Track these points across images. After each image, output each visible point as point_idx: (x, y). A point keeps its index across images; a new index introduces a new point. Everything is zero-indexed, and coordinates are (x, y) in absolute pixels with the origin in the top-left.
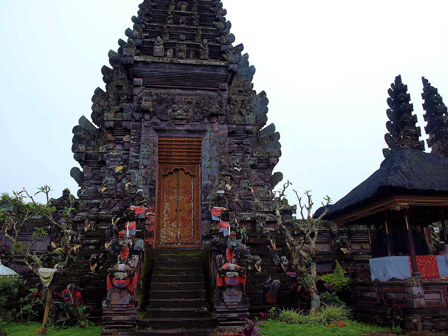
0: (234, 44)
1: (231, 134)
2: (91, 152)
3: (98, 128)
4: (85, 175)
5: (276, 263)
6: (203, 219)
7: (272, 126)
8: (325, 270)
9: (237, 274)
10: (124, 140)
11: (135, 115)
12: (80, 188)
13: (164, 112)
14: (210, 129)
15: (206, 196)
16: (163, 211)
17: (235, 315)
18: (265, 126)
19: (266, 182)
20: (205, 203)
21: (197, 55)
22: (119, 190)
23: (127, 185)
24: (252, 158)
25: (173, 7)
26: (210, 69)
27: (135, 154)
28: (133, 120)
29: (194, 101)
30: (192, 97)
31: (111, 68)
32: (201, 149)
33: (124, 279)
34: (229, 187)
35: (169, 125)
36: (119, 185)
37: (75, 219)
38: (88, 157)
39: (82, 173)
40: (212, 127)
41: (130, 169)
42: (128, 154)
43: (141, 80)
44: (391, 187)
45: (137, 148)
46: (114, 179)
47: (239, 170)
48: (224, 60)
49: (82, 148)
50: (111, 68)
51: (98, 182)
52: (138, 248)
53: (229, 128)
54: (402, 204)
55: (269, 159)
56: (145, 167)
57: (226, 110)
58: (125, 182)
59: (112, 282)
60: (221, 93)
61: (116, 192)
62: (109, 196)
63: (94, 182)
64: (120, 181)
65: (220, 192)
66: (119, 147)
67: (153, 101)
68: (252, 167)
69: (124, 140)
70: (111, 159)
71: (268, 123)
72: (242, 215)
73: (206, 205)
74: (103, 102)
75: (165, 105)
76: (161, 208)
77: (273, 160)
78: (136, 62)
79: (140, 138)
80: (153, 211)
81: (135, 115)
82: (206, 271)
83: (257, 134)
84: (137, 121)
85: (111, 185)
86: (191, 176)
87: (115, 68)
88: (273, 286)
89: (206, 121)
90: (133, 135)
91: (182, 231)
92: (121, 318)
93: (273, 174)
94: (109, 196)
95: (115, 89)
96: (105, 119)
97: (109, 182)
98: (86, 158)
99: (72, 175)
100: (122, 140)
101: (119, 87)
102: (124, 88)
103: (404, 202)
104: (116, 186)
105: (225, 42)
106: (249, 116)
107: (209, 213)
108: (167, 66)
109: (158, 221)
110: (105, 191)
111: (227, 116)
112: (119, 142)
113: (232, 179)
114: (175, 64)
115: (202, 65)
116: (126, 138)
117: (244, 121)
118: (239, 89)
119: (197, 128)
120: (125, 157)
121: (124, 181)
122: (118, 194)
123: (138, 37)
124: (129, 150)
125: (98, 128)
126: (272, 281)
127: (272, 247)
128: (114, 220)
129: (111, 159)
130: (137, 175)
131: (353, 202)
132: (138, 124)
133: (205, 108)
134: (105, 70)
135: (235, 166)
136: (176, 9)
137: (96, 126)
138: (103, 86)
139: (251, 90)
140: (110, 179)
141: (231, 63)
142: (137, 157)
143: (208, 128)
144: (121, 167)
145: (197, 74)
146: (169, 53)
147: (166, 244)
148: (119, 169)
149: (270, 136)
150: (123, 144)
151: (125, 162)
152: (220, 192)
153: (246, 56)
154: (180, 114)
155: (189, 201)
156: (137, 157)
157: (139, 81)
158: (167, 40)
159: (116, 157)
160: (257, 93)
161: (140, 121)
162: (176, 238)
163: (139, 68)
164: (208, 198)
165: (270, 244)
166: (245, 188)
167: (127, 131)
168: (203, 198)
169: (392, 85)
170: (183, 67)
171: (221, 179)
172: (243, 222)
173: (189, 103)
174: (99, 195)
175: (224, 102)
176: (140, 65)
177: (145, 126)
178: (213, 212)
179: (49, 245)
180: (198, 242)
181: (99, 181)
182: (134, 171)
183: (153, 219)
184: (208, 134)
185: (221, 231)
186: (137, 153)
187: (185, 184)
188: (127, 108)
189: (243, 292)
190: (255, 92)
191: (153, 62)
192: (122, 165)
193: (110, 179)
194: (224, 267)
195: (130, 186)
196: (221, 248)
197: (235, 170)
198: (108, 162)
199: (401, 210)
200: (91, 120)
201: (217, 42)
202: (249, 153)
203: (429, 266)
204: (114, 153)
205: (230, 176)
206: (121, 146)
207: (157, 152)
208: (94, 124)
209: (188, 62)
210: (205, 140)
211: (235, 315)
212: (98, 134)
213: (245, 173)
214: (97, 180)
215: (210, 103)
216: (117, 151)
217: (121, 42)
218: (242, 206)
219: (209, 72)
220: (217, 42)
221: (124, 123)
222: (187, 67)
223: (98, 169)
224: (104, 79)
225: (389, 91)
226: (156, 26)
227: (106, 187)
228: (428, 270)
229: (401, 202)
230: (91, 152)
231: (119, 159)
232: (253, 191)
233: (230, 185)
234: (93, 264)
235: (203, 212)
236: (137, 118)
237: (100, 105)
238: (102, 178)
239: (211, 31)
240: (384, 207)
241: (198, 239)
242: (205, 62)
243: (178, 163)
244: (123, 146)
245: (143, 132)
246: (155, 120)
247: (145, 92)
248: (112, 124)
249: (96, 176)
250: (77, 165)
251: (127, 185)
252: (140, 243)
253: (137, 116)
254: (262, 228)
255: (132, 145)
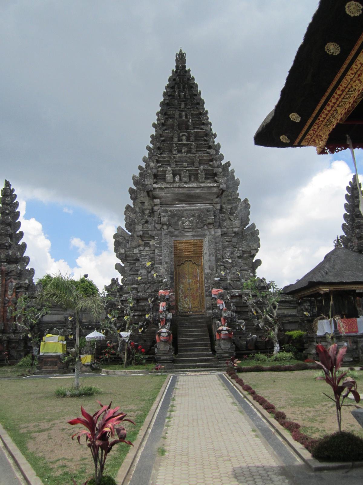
0: (223, 162)
1: (223, 234)
2: (129, 253)
3: (130, 234)
4: (126, 269)
5: (256, 324)
6: (207, 296)
7: (253, 226)
8: (293, 328)
9: (227, 332)
10: (151, 244)
11: (157, 226)
12: (122, 277)
13: (176, 224)
14: (209, 233)
15: (208, 281)
16: (179, 290)
17: (227, 355)
18: (248, 226)
19: (249, 267)
20: (207, 285)
21: (197, 179)
22: (150, 278)
23: (155, 275)
24: (238, 252)
25: (176, 139)
26: (206, 189)
27: (159, 254)
28: (156, 230)
29: (197, 215)
30: (195, 212)
31: (135, 188)
32: (202, 247)
33: (166, 337)
34: (223, 273)
35: (180, 232)
36: (149, 275)
37: (122, 299)
38: (126, 256)
39: (124, 267)
40: (210, 232)
41: (157, 264)
42: (154, 253)
43: (159, 200)
44: (314, 282)
45: (160, 249)
46: (146, 271)
47: (230, 261)
48: (216, 182)
49: (122, 251)
50: (135, 188)
51: (136, 273)
52: (169, 318)
53: (222, 231)
54: (325, 290)
55: (250, 251)
56: (166, 263)
57: (219, 218)
58: (153, 273)
59: (159, 338)
60: (215, 205)
61: (148, 280)
62: (143, 283)
63: (132, 273)
64: (150, 272)
65: (216, 279)
66: (147, 249)
67: (169, 216)
68: (239, 257)
69: (151, 244)
70: (143, 258)
71: (250, 223)
72: (233, 292)
73: (208, 286)
74: (132, 215)
75: (176, 218)
76: (178, 288)
77: (253, 252)
78: (154, 189)
79: (161, 242)
80: (173, 292)
81: (157, 226)
82: (210, 330)
83: (242, 232)
84: (158, 230)
85: (144, 275)
86: (197, 265)
87: (138, 189)
88: (252, 339)
89: (206, 228)
90: (156, 241)
91: (193, 303)
92: (165, 357)
93: (254, 261)
94: (143, 283)
95: (139, 205)
96: (137, 230)
97: (143, 273)
98: (125, 257)
99: (116, 268)
100: (149, 244)
101: (143, 203)
102: (146, 204)
103: (326, 288)
104: (147, 276)
105: (216, 165)
106: (236, 221)
107: (210, 292)
108: (176, 189)
109: (176, 297)
110: (140, 279)
111: (220, 223)
112: (146, 245)
113: (225, 267)
114: (182, 187)
115: (201, 187)
116: (151, 243)
117: (232, 225)
118: (227, 198)
119: (199, 233)
120: (152, 255)
121: (153, 272)
122: (149, 281)
123: (154, 168)
124: (154, 250)
125: (130, 234)
126: (251, 336)
127: (253, 313)
128: (150, 300)
129: (143, 258)
130: (161, 268)
131: (300, 287)
132: (159, 232)
133: (204, 219)
134: (131, 191)
135: (227, 258)
136: (179, 140)
137: (129, 233)
138: (131, 203)
139: (237, 198)
140: (143, 271)
141: (221, 184)
142: (160, 256)
143: (207, 232)
144: (150, 263)
145: (197, 193)
146: (177, 179)
147: (182, 312)
148: (148, 264)
149: (252, 233)
150: (150, 247)
151: (152, 259)
152: (216, 279)
153: (233, 172)
154: (188, 225)
155: (196, 283)
156: (160, 256)
157: (157, 201)
158: (175, 168)
159: (146, 256)
160: (242, 200)
161: (160, 230)
162: (189, 308)
163: (157, 192)
164: (209, 281)
165: (251, 311)
166: (234, 273)
167: (153, 237)
168: (206, 282)
169: (350, 183)
170: (187, 189)
171: (217, 268)
172: (233, 297)
173: (193, 216)
174: (137, 283)
175: (217, 212)
176: (158, 190)
177: (164, 234)
178: (213, 292)
179: (106, 316)
180: (204, 311)
181: (136, 272)
182: (159, 265)
183: (174, 297)
184: (207, 237)
185: (218, 305)
186: (160, 253)
187: (193, 271)
188: (150, 221)
189: (231, 342)
190: (240, 199)
191: (166, 188)
192: (150, 261)
193: (143, 271)
194: (220, 328)
195: (157, 276)
196: (218, 317)
197: (227, 261)
198: (141, 259)
199: (324, 293)
200: (125, 229)
201: (210, 166)
202: (236, 248)
203: (351, 325)
204: (144, 253)
205: (224, 265)
206: (148, 248)
207: (173, 251)
208: (127, 231)
209: (191, 185)
210: (206, 242)
211: (227, 355)
212: (131, 238)
213: (234, 263)
214: (134, 271)
215: (208, 215)
216: (146, 251)
217: (140, 168)
218: (233, 286)
219: (206, 191)
220: (210, 166)
221: (150, 232)
222: (190, 189)
223: (134, 264)
224: (131, 197)
225: (348, 188)
226: (166, 157)
227: (141, 277)
228: (350, 327)
229: (324, 288)
230: (129, 253)
231: (148, 257)
232: (240, 275)
233: (224, 271)
234: (141, 328)
235: (206, 291)
236: (158, 228)
237: (130, 218)
238: (138, 271)
239: (206, 156)
240: (316, 291)
241: (204, 308)
242: (203, 185)
243: (188, 257)
244: (150, 248)
245: (163, 238)
246: (171, 229)
247: (163, 210)
248: (141, 233)
249: (133, 269)
250: (119, 261)
251: (155, 275)
252: (170, 316)
253: (158, 227)
254: (246, 301)
255: (156, 248)
